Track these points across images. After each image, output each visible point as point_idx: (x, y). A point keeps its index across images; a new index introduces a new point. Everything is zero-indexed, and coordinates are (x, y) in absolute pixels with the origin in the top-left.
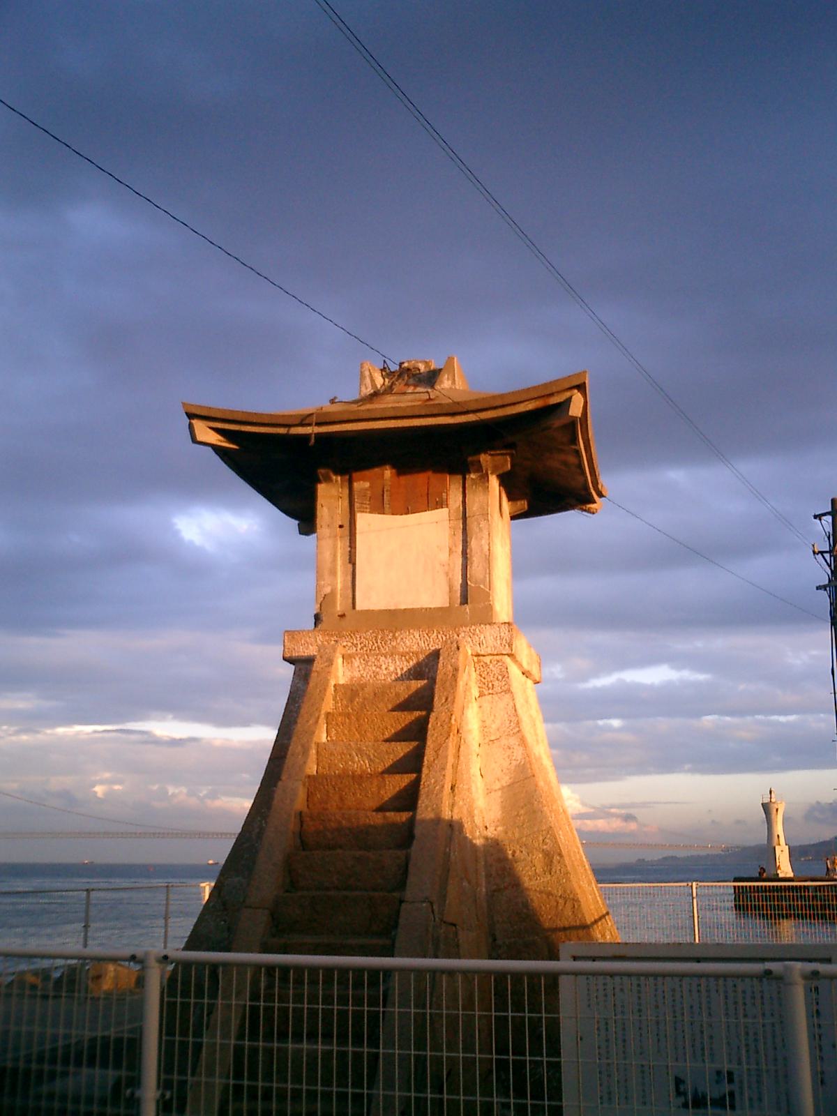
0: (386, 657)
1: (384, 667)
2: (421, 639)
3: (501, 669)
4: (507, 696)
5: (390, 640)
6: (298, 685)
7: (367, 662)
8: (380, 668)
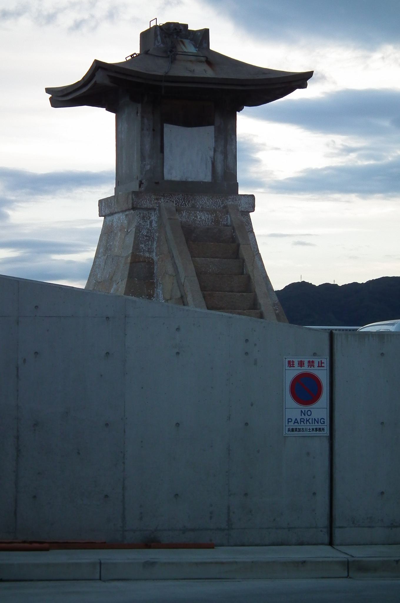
0: (199, 212)
1: (199, 217)
2: (207, 201)
3: (247, 220)
4: (252, 234)
5: (191, 200)
6: (140, 222)
7: (190, 214)
8: (197, 218)
